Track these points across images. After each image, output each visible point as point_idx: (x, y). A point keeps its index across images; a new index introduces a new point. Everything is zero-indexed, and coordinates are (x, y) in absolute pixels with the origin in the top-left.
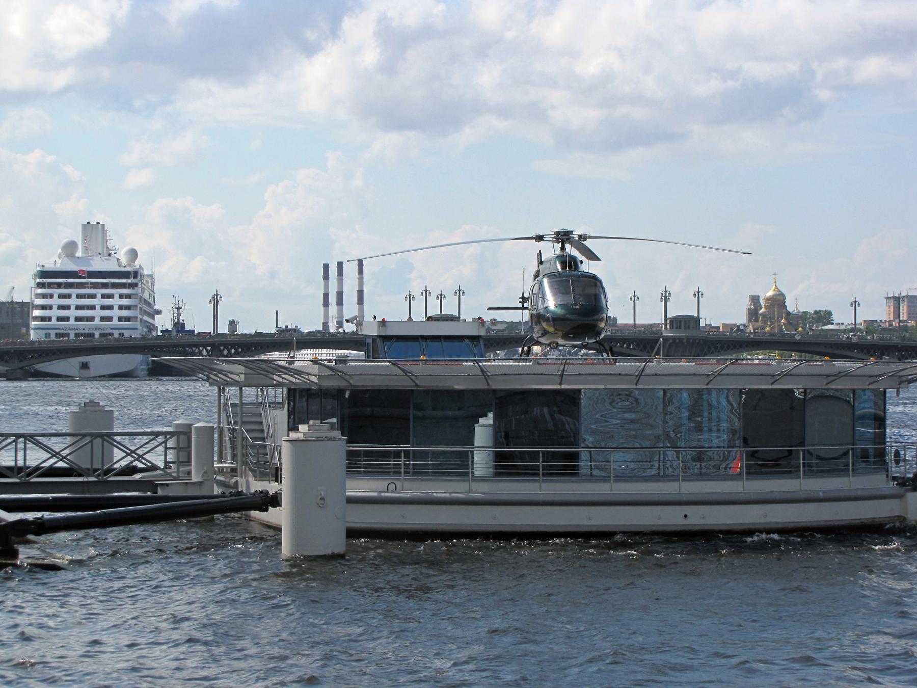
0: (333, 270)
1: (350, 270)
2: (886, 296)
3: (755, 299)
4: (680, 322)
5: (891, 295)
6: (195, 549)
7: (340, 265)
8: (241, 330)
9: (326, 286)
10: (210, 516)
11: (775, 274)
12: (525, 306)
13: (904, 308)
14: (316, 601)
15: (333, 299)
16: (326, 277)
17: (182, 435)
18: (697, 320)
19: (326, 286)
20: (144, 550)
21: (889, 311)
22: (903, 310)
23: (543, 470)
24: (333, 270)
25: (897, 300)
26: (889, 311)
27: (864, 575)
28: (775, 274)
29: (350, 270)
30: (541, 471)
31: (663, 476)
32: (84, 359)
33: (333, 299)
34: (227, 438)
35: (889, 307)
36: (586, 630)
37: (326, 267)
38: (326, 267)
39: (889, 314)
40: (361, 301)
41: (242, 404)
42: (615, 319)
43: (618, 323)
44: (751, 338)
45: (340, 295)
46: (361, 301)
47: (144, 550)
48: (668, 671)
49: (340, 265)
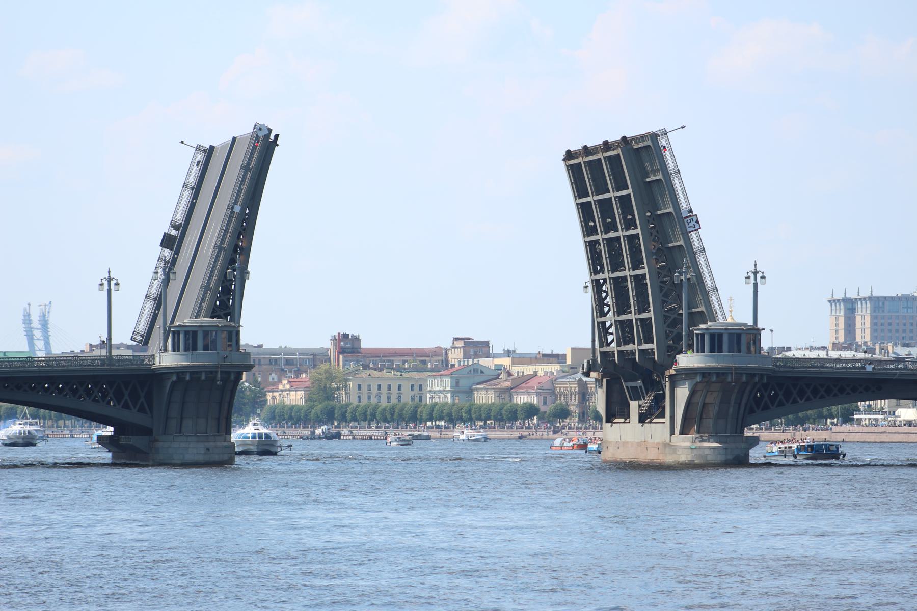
2: (830, 298)
4: (195, 333)
5: (839, 295)
8: (553, 353)
11: (731, 300)
14: (869, 520)
17: (704, 400)
18: (754, 333)
20: (800, 590)
21: (837, 325)
22: (863, 324)
23: (608, 191)
25: (850, 306)
26: (837, 325)
28: (731, 300)
30: (611, 195)
35: (837, 318)
39: (837, 331)
43: (362, 346)
44: (869, 373)
47: (800, 590)
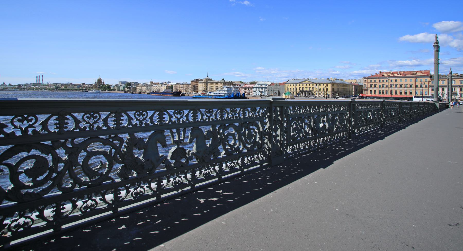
0: (38, 77)
6: (276, 79)
7: (39, 76)
9: (37, 79)
10: (279, 128)
12: (254, 92)
13: (121, 83)
15: (38, 80)
19: (37, 79)
24: (38, 77)
25: (120, 82)
27: (177, 191)
31: (353, 85)
33: (38, 80)
37: (37, 76)
38: (37, 76)
40: (42, 81)
45: (39, 80)
46: (42, 81)
48: (294, 97)
49: (39, 76)
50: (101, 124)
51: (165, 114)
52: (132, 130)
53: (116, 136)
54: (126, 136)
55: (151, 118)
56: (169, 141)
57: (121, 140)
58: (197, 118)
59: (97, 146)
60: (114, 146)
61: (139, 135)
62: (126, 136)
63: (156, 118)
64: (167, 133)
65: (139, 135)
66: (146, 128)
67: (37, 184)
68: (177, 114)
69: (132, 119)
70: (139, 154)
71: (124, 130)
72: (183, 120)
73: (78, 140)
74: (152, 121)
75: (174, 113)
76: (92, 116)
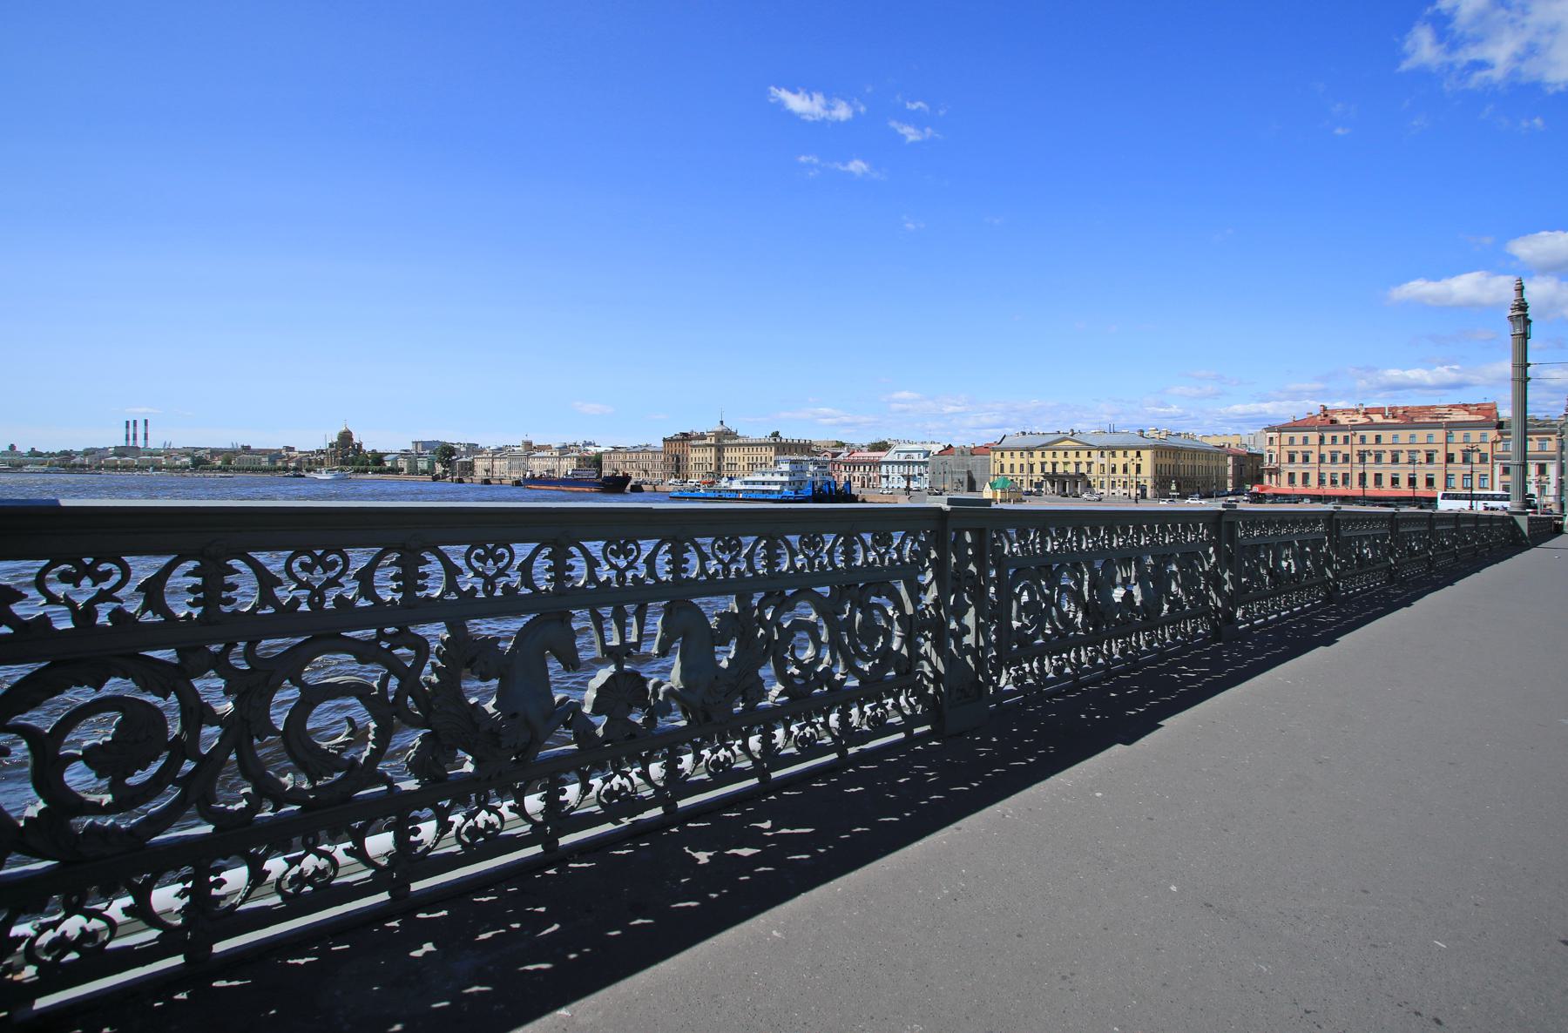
0: (131, 425)
1: (141, 425)
3: (1510, 317)
9: (127, 431)
15: (131, 437)
16: (127, 427)
19: (127, 431)
24: (131, 425)
25: (416, 443)
29: (141, 425)
31: (1229, 456)
32: (1412, 432)
33: (131, 437)
34: (18, 478)
36: (43, 929)
37: (128, 422)
38: (128, 422)
41: (1527, 427)
42: (360, 445)
49: (135, 422)
50: (350, 590)
51: (574, 556)
52: (458, 610)
53: (403, 631)
54: (436, 633)
55: (526, 568)
56: (587, 648)
57: (421, 646)
58: (686, 570)
59: (335, 668)
60: (394, 667)
61: (484, 628)
62: (436, 633)
63: (541, 566)
64: (580, 620)
65: (484, 628)
66: (508, 605)
67: (126, 800)
68: (616, 554)
69: (460, 571)
70: (483, 695)
71: (431, 610)
72: (635, 576)
73: (272, 646)
74: (528, 580)
75: (604, 551)
76: (319, 561)
